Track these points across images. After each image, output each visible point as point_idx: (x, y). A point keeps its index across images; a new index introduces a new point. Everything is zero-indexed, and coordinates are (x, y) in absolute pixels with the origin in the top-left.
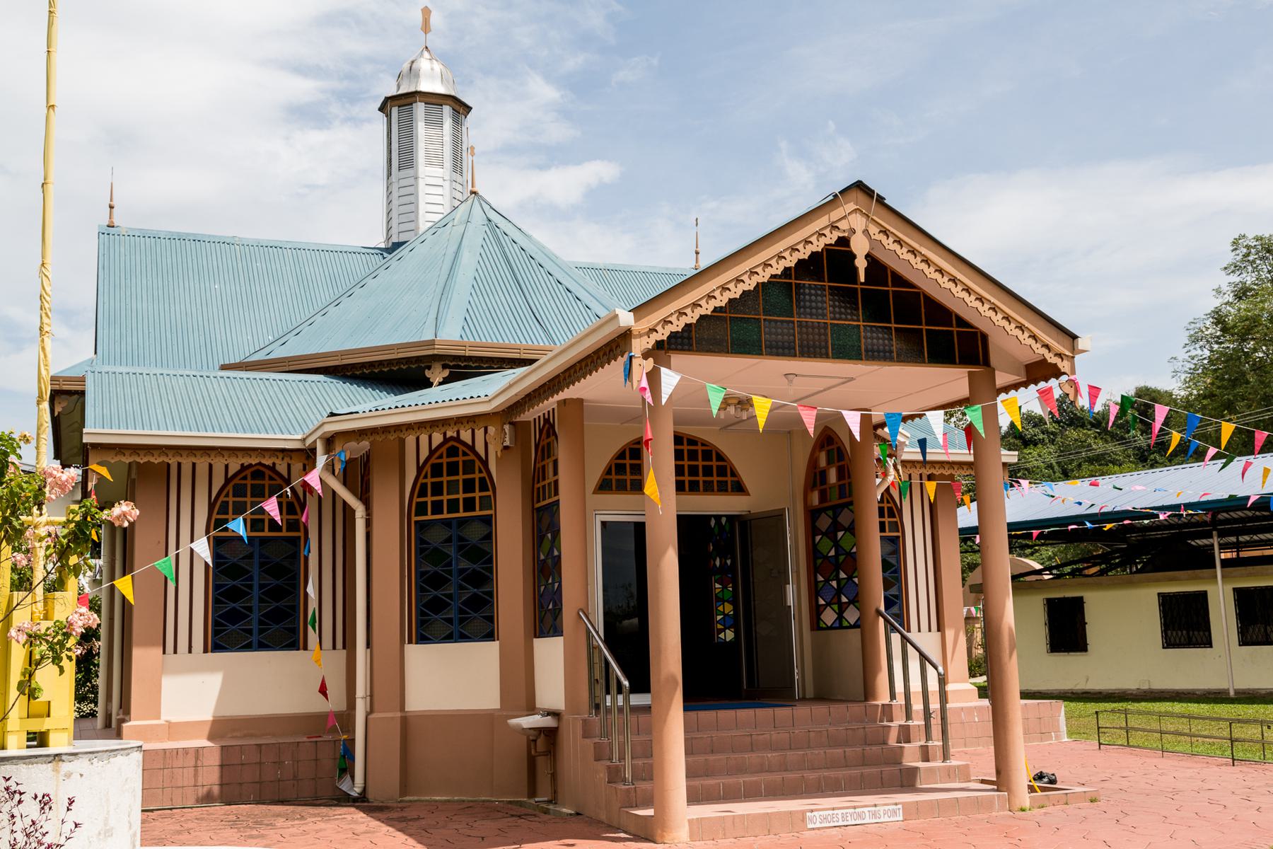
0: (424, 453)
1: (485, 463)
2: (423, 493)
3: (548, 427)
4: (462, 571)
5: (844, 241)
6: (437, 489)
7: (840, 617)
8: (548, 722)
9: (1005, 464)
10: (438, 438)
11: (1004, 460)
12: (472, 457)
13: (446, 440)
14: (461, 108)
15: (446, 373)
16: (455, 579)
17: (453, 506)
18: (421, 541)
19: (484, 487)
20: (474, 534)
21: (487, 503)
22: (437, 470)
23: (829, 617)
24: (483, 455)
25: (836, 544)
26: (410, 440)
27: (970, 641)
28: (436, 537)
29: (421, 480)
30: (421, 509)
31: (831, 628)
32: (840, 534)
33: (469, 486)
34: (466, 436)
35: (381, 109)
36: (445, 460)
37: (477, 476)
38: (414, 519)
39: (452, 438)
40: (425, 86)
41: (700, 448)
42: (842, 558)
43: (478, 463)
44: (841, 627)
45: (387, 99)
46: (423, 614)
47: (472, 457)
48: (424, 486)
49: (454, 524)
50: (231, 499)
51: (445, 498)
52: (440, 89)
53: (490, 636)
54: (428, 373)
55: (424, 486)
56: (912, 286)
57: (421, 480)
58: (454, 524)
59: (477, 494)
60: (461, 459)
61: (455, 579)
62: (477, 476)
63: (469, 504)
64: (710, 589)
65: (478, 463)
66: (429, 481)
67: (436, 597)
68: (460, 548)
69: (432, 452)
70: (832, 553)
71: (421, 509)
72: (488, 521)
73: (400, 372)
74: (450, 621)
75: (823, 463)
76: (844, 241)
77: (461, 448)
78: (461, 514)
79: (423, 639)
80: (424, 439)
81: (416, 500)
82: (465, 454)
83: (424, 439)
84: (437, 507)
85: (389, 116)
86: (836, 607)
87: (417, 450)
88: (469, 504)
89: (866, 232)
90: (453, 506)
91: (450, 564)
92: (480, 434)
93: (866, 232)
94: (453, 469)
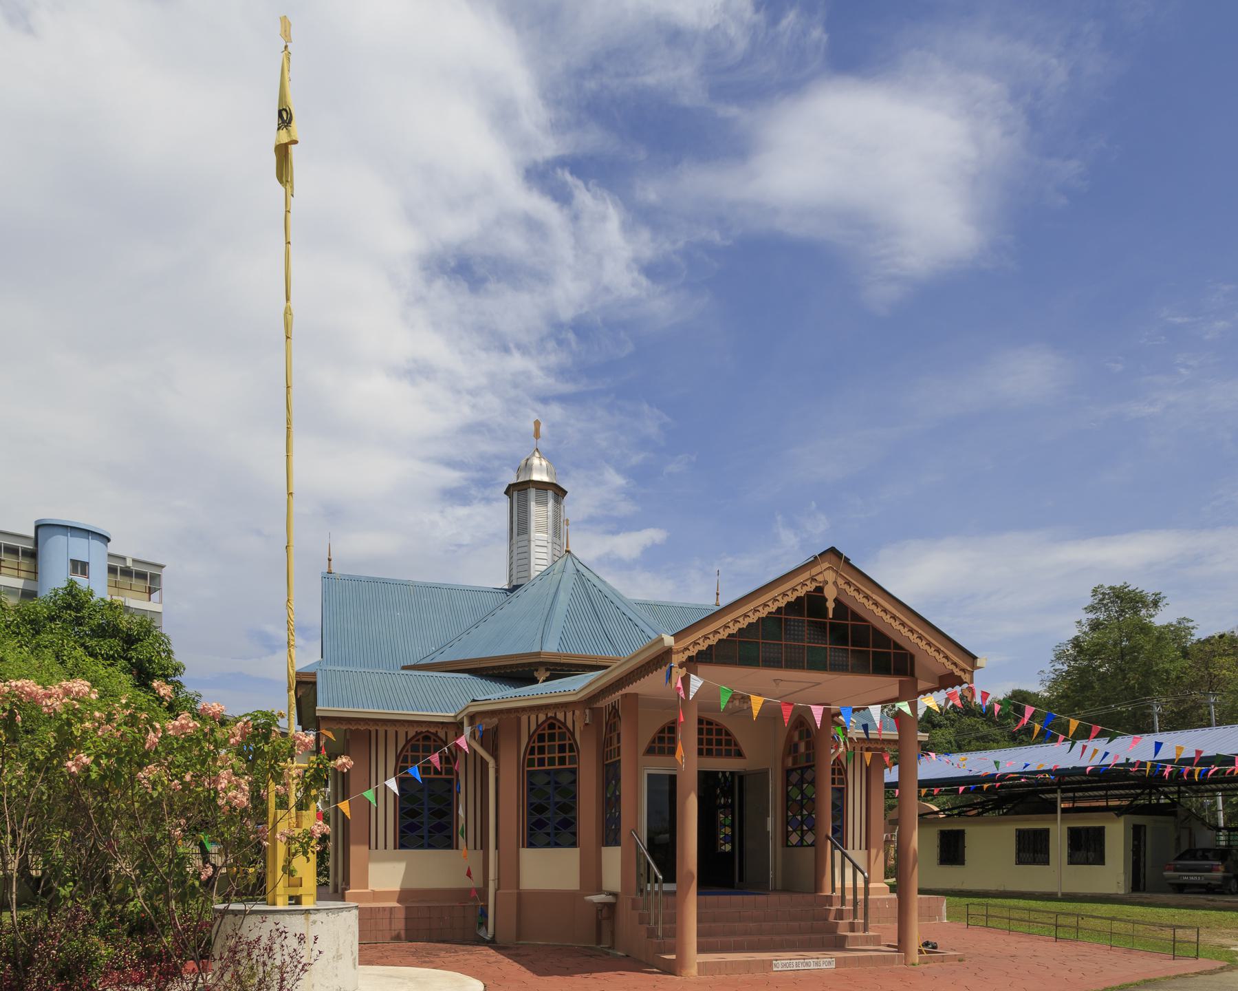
0: (533, 727)
1: (573, 734)
2: (532, 752)
3: (614, 711)
4: (556, 803)
5: (820, 590)
8: (610, 899)
10: (542, 717)
13: (548, 718)
15: (548, 674)
20: (564, 779)
21: (573, 760)
22: (541, 738)
23: (794, 839)
24: (570, 726)
33: (562, 748)
34: (560, 716)
36: (547, 732)
37: (567, 742)
41: (714, 727)
44: (802, 845)
45: (510, 486)
50: (410, 754)
51: (546, 756)
54: (536, 674)
55: (533, 748)
60: (557, 731)
62: (567, 742)
63: (562, 761)
69: (538, 726)
72: (574, 772)
73: (517, 672)
74: (548, 834)
76: (820, 590)
77: (557, 724)
78: (557, 767)
80: (533, 718)
83: (533, 718)
87: (529, 725)
88: (562, 761)
89: (835, 583)
92: (569, 715)
93: (835, 583)
94: (552, 737)
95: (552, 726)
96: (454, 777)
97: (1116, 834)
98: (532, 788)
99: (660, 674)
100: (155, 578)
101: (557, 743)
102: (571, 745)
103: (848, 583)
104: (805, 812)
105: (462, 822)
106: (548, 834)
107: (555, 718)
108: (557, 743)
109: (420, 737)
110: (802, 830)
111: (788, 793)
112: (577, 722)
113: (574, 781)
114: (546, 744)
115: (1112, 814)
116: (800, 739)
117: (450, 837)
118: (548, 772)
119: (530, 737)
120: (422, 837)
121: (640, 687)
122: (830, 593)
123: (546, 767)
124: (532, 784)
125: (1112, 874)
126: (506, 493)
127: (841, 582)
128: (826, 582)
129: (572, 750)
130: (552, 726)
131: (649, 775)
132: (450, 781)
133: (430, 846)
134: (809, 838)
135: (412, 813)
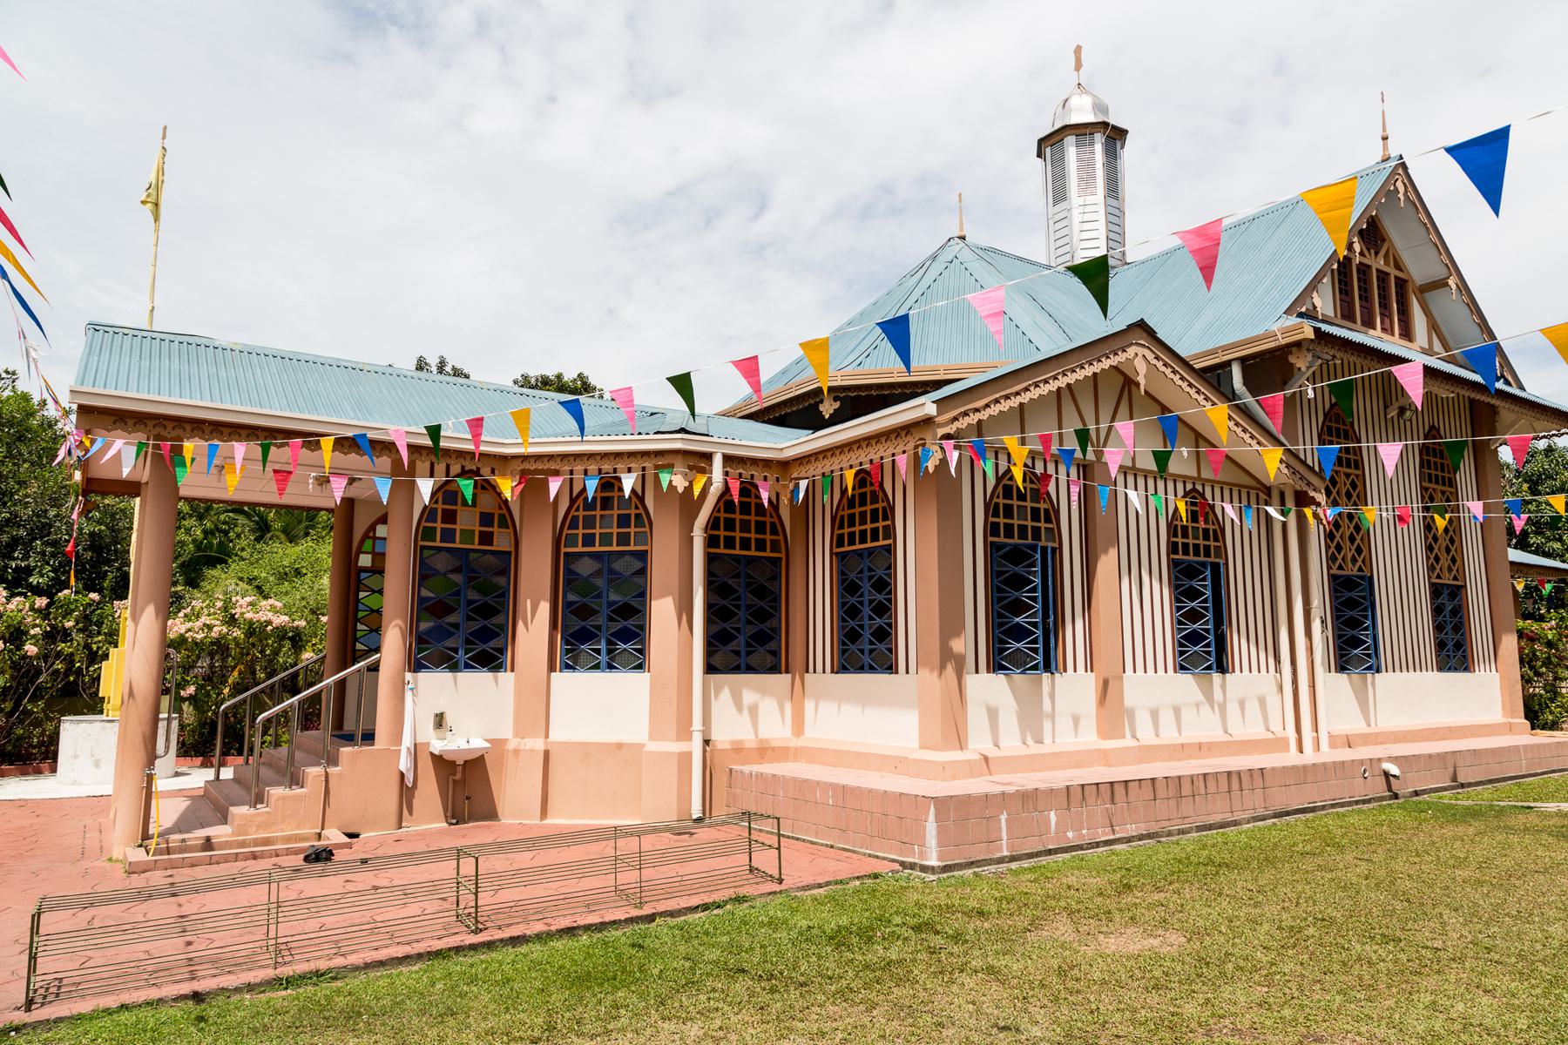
4: (470, 602)
9: (1512, 563)
11: (1511, 558)
14: (1115, 136)
16: (742, 614)
17: (605, 540)
18: (568, 571)
20: (624, 567)
21: (646, 538)
27: (638, 832)
28: (585, 568)
29: (573, 513)
38: (563, 550)
40: (1076, 119)
49: (866, 554)
50: (581, 513)
52: (1091, 118)
55: (575, 518)
58: (866, 554)
59: (632, 530)
61: (742, 614)
63: (624, 539)
67: (1194, 631)
68: (748, 585)
71: (571, 541)
72: (643, 556)
74: (737, 653)
78: (615, 548)
81: (424, 524)
84: (730, 543)
91: (738, 598)
96: (783, 555)
98: (572, 580)
100: (1201, 232)
102: (638, 516)
103: (1157, 358)
105: (1316, 626)
106: (737, 653)
118: (597, 556)
120: (598, 651)
123: (597, 548)
124: (843, 573)
127: (1150, 356)
132: (775, 562)
135: (583, 612)
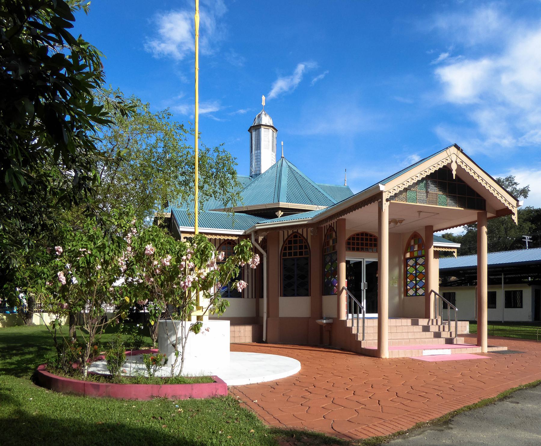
0: (286, 237)
1: (307, 240)
2: (285, 249)
3: (331, 228)
5: (450, 164)
6: (290, 248)
7: (416, 292)
8: (330, 321)
10: (290, 232)
12: (302, 238)
13: (293, 232)
15: (282, 213)
17: (295, 254)
19: (306, 248)
22: (290, 242)
23: (411, 292)
24: (306, 237)
25: (416, 269)
26: (281, 232)
30: (285, 255)
31: (412, 296)
32: (418, 266)
33: (301, 247)
34: (300, 231)
35: (249, 131)
36: (293, 239)
37: (304, 244)
39: (295, 232)
41: (373, 238)
42: (418, 274)
43: (304, 240)
44: (416, 295)
45: (251, 127)
46: (284, 287)
47: (302, 238)
48: (286, 247)
51: (293, 251)
53: (307, 295)
54: (276, 213)
55: (286, 247)
56: (464, 182)
57: (285, 245)
60: (298, 239)
62: (304, 244)
63: (301, 253)
64: (142, 313)
65: (304, 240)
66: (287, 245)
69: (288, 236)
70: (414, 272)
72: (307, 259)
73: (269, 213)
75: (412, 243)
76: (450, 164)
77: (298, 235)
78: (298, 256)
79: (285, 295)
80: (286, 232)
81: (283, 251)
82: (300, 237)
83: (286, 232)
84: (290, 254)
85: (251, 133)
86: (414, 289)
87: (283, 237)
88: (301, 253)
89: (456, 162)
90: (295, 254)
92: (305, 230)
93: (456, 162)
94: (296, 242)
95: (295, 236)
97: (528, 295)
99: (374, 206)
101: (298, 245)
104: (418, 279)
107: (297, 232)
108: (298, 245)
109: (226, 242)
110: (416, 288)
111: (407, 270)
112: (308, 234)
113: (307, 264)
114: (293, 245)
115: (526, 285)
116: (415, 244)
117: (307, 290)
119: (284, 242)
121: (347, 216)
122: (454, 167)
125: (526, 312)
126: (249, 131)
128: (452, 162)
129: (306, 248)
130: (295, 236)
131: (361, 262)
133: (298, 295)
134: (421, 292)
